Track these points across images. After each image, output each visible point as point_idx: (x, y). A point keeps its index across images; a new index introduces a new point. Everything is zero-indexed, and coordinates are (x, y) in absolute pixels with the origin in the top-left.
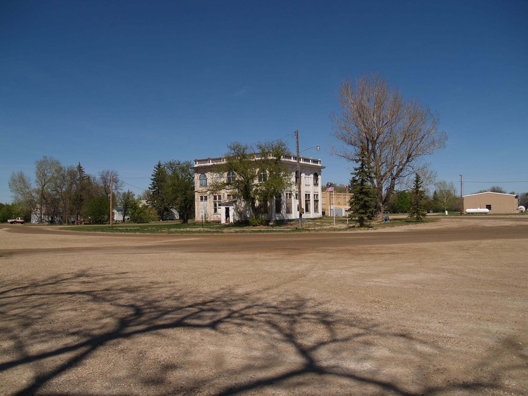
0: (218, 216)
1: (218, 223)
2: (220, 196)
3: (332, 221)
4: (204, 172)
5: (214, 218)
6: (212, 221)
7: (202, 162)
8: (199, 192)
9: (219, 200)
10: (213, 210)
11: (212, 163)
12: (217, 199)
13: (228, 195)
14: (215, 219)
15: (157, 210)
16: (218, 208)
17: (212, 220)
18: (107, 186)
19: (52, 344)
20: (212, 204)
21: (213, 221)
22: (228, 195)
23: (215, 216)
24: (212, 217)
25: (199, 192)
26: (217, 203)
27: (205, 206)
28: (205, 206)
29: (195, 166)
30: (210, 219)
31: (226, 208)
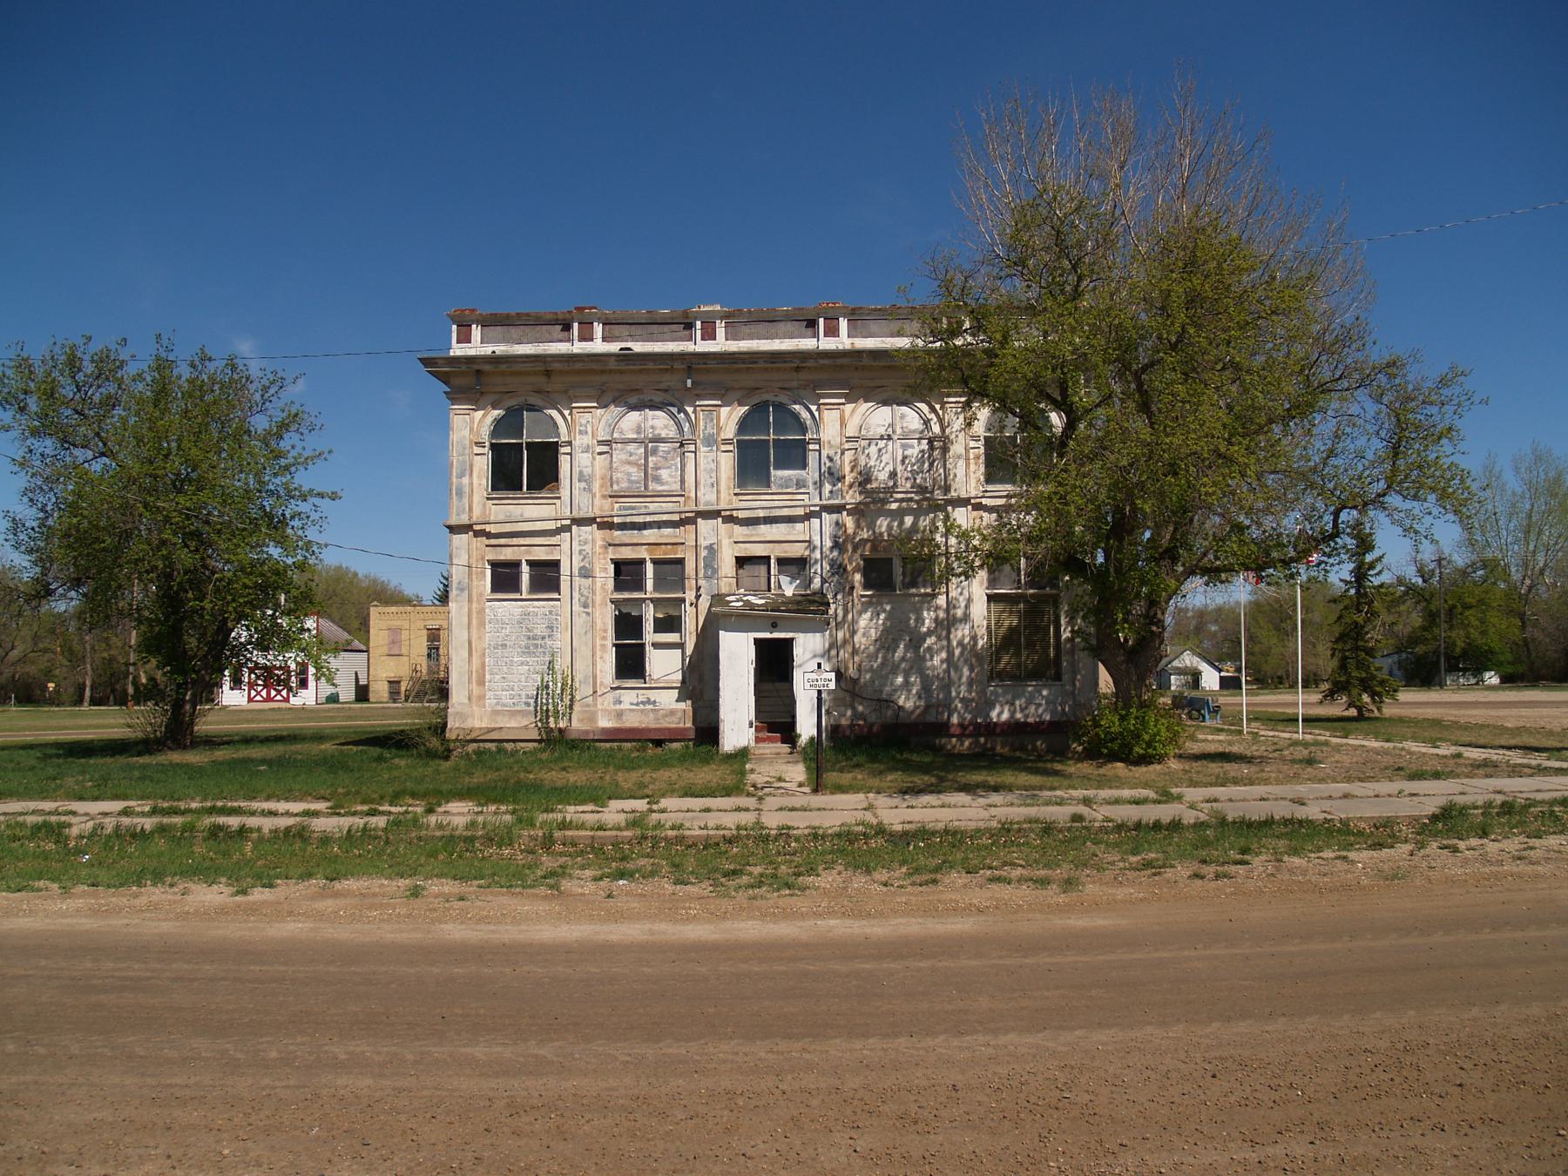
0: (653, 695)
1: (658, 743)
2: (149, 661)
3: (1250, 709)
4: (534, 400)
5: (620, 714)
6: (604, 730)
7: (515, 332)
8: (489, 535)
9: (656, 588)
10: (607, 663)
11: (604, 339)
12: (650, 584)
13: (741, 562)
14: (632, 721)
15: (1207, 717)
16: (656, 646)
17: (605, 723)
18: (911, 871)
19: (528, 398)
20: (606, 618)
21: (617, 736)
22: (741, 562)
23: (629, 698)
24: (606, 702)
25: (489, 535)
26: (649, 614)
27: (540, 630)
28: (540, 630)
29: (458, 350)
30: (592, 718)
31: (757, 641)
